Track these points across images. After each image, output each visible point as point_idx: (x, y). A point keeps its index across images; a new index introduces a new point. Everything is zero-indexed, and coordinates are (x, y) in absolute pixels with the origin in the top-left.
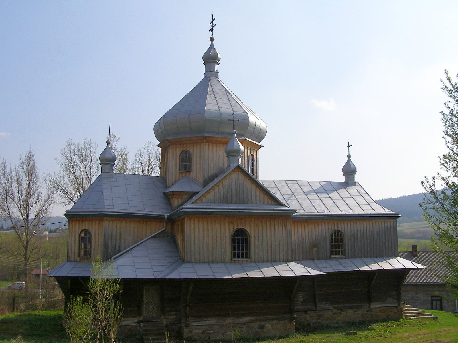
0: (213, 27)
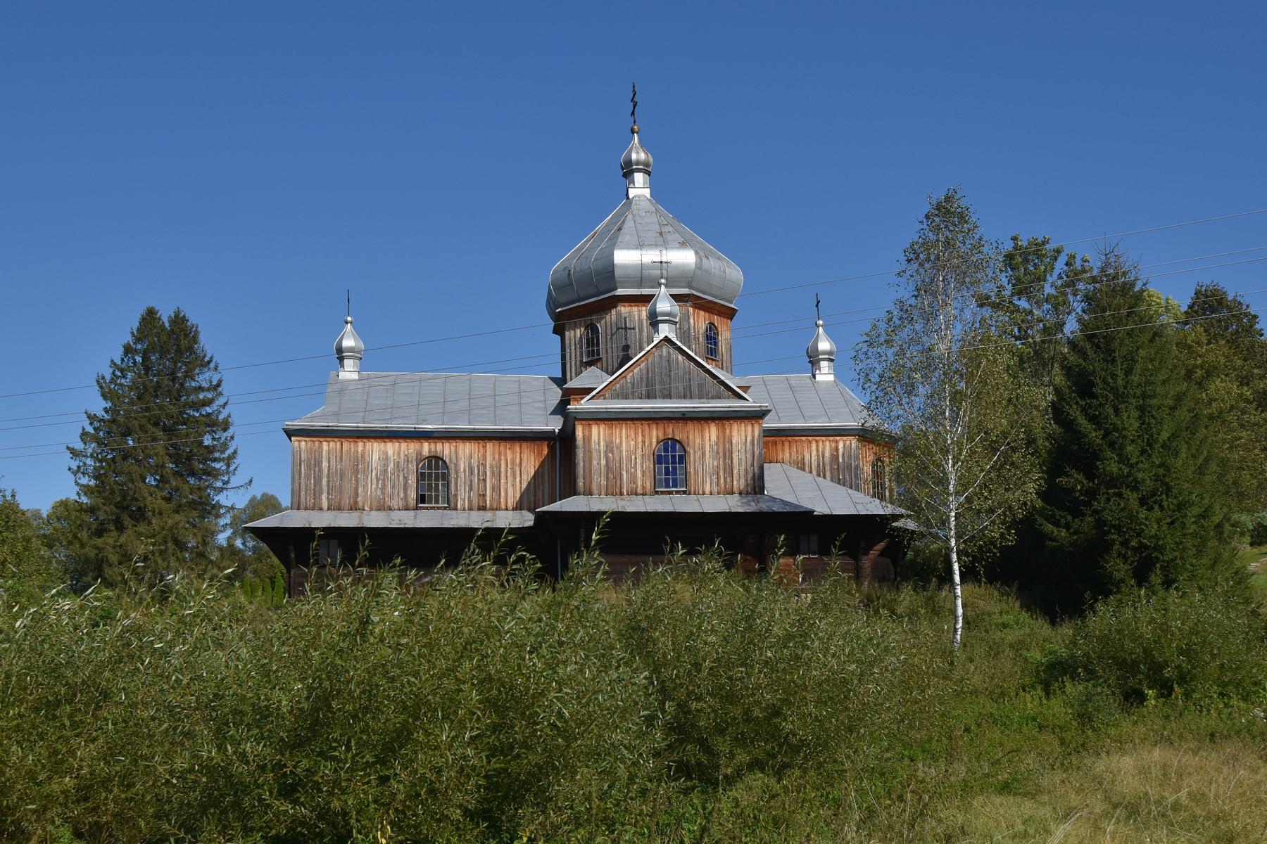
0: (634, 107)
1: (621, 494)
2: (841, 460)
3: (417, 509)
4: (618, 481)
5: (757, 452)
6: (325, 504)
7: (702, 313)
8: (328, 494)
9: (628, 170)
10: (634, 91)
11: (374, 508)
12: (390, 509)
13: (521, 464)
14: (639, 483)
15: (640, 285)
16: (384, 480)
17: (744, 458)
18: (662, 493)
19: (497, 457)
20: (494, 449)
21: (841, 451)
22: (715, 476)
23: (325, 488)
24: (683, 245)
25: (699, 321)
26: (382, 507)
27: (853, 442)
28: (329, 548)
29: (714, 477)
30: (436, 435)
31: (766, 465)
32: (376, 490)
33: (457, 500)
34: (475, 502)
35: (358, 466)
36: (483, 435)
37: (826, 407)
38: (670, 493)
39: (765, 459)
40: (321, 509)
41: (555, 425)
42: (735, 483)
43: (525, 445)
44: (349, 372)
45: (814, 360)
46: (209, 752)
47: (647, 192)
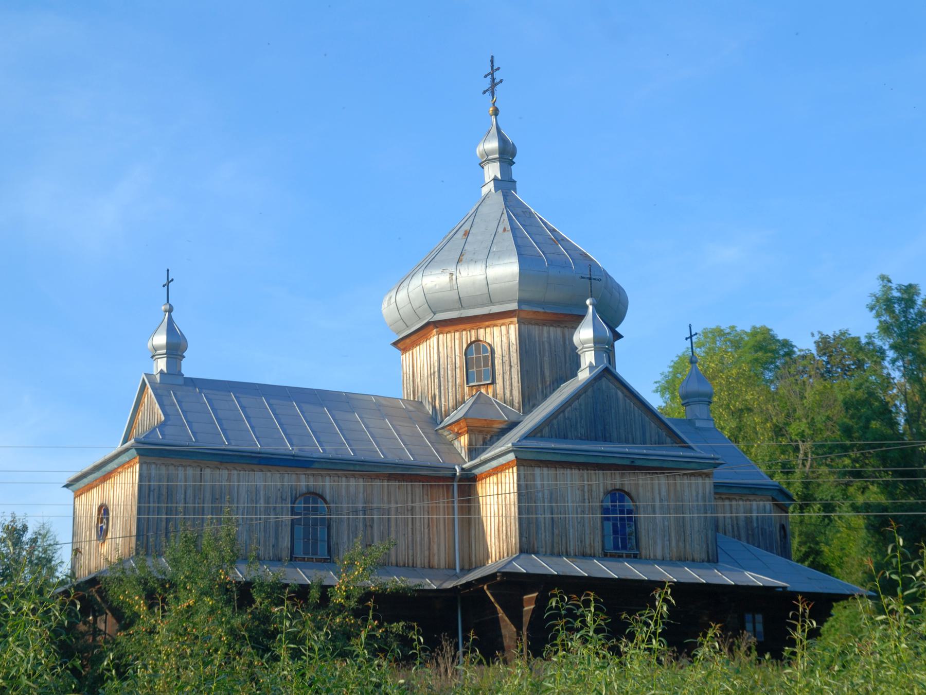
2: (755, 525)
42: (688, 546)
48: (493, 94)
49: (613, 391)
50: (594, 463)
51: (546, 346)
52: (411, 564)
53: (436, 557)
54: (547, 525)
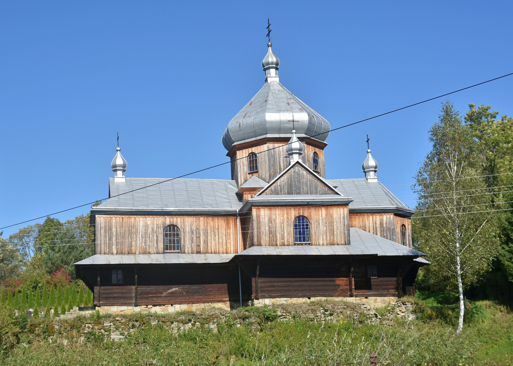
1: (277, 245)
2: (385, 226)
3: (164, 253)
4: (275, 238)
5: (346, 223)
6: (115, 251)
7: (310, 147)
8: (116, 246)
9: (266, 68)
10: (268, 23)
11: (141, 253)
12: (150, 253)
13: (218, 229)
14: (286, 239)
15: (279, 131)
16: (146, 238)
17: (339, 225)
18: (298, 244)
19: (206, 225)
20: (204, 221)
21: (385, 221)
22: (325, 236)
23: (114, 242)
24: (302, 109)
25: (310, 151)
26: (145, 252)
27: (392, 216)
28: (117, 275)
29: (324, 236)
30: (174, 213)
31: (351, 228)
32: (142, 243)
33: (185, 248)
34: (195, 250)
35: (132, 231)
36: (198, 213)
37: (375, 197)
38: (302, 244)
39: (350, 226)
40: (113, 254)
41: (236, 207)
42: (335, 239)
43: (220, 218)
44: (119, 179)
45: (365, 171)
46: (267, 325)
47: (277, 79)
48: (269, 37)
49: (302, 172)
50: (327, 194)
51: (282, 152)
52: (218, 252)
53: (229, 249)
54: (267, 233)
